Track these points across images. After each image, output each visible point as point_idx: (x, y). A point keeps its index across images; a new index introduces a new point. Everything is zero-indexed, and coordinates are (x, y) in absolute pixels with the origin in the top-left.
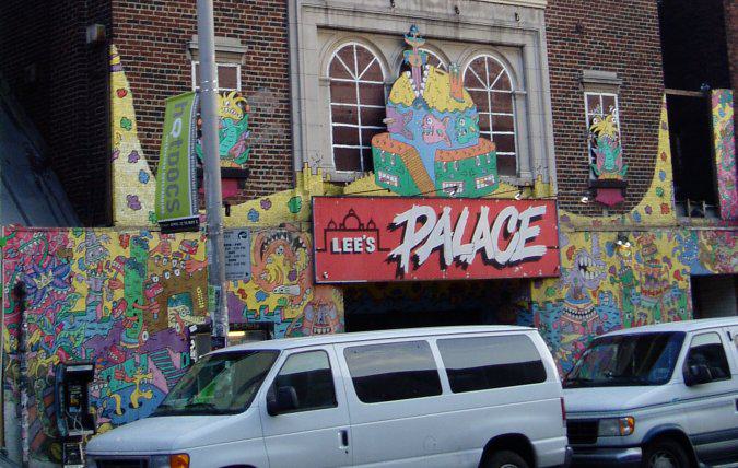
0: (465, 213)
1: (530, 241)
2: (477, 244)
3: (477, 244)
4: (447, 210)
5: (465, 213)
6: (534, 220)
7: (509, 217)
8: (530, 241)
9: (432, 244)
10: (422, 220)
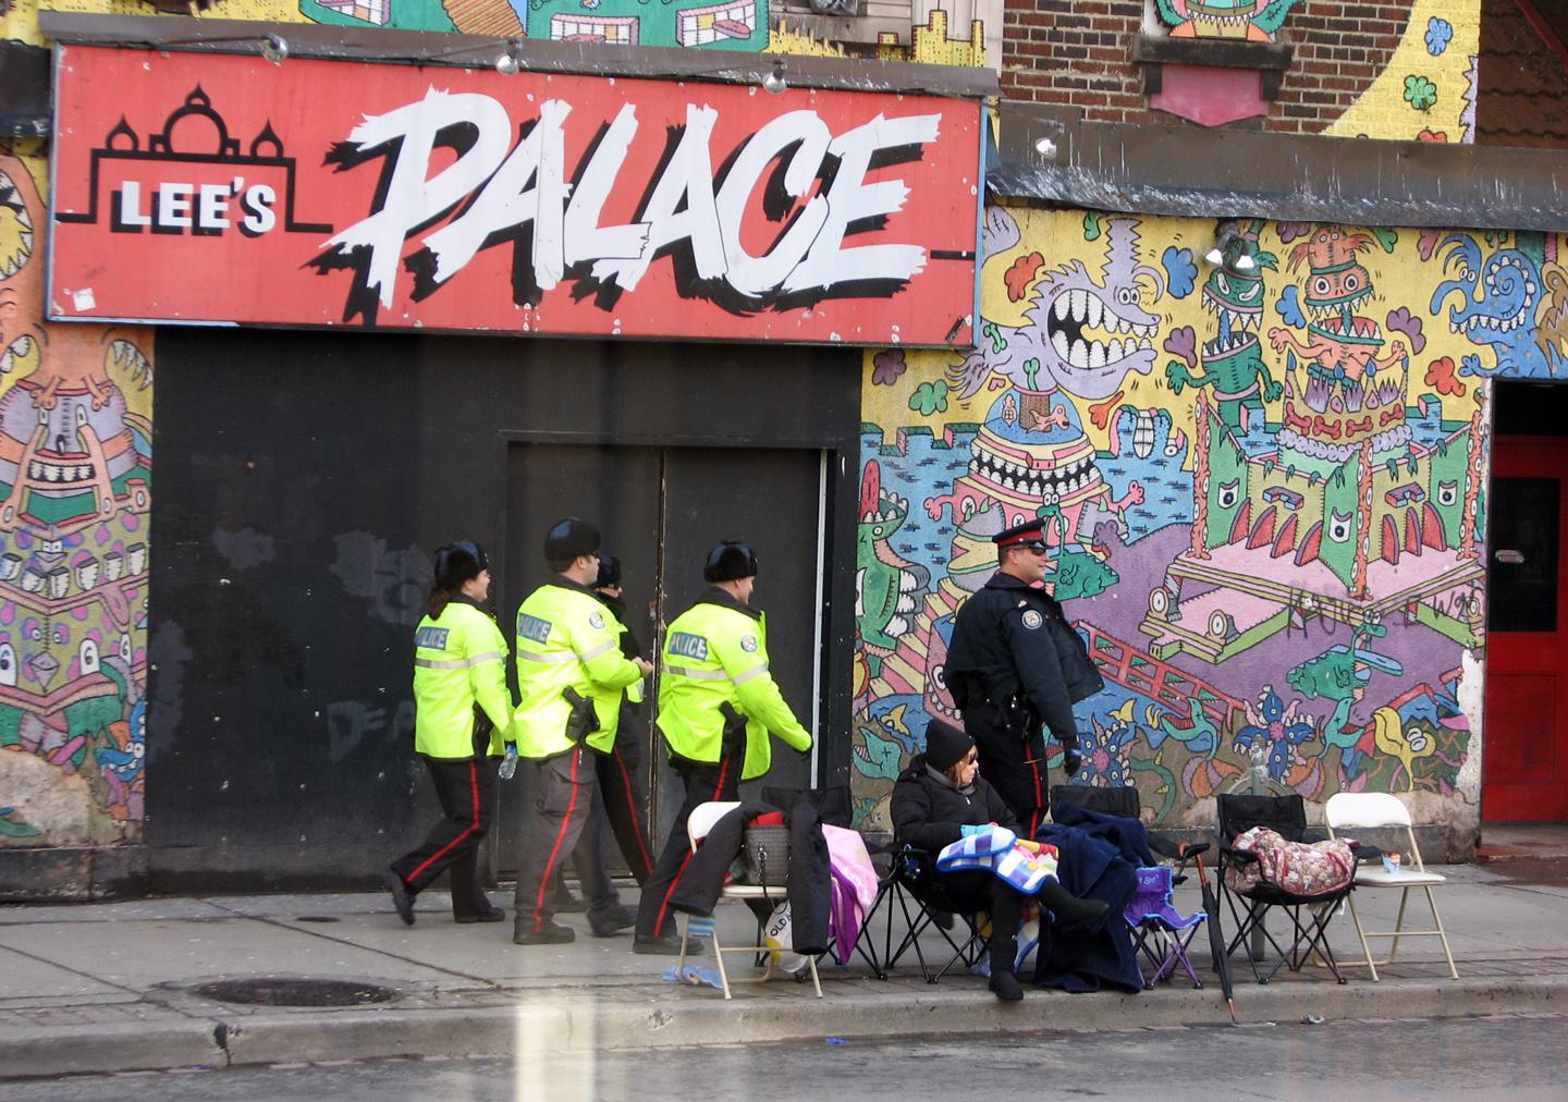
0: (625, 126)
1: (864, 229)
2: (662, 225)
3: (662, 225)
4: (554, 113)
5: (625, 126)
6: (885, 161)
7: (796, 145)
8: (864, 229)
9: (494, 214)
10: (458, 139)
